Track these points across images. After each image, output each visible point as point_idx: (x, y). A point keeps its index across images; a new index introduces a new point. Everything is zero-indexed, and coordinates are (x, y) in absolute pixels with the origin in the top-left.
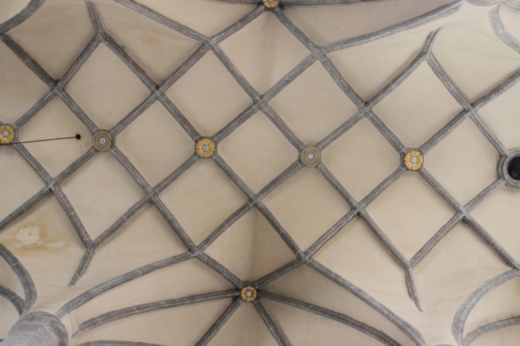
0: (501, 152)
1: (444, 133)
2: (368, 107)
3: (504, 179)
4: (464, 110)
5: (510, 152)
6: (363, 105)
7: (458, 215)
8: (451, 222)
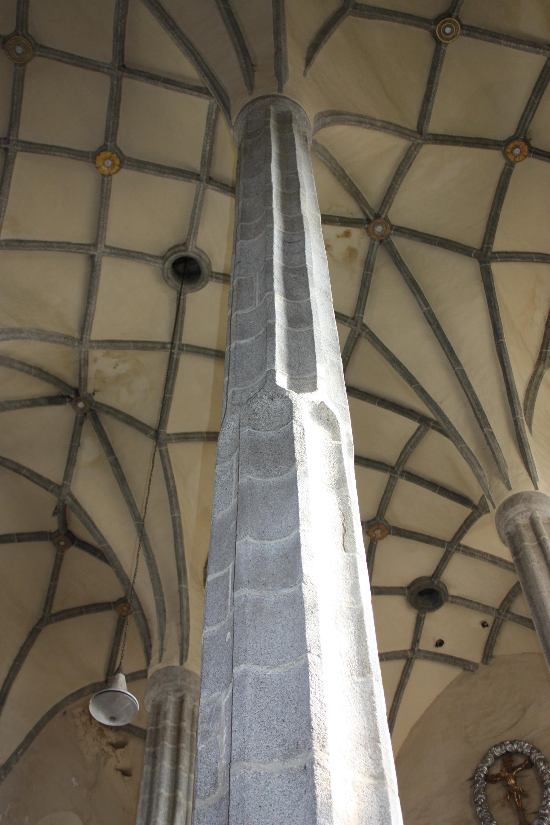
0: (188, 242)
1: (159, 171)
2: (120, 73)
3: (164, 264)
4: (199, 175)
5: (194, 249)
6: (117, 65)
7: (92, 248)
8: (78, 247)
